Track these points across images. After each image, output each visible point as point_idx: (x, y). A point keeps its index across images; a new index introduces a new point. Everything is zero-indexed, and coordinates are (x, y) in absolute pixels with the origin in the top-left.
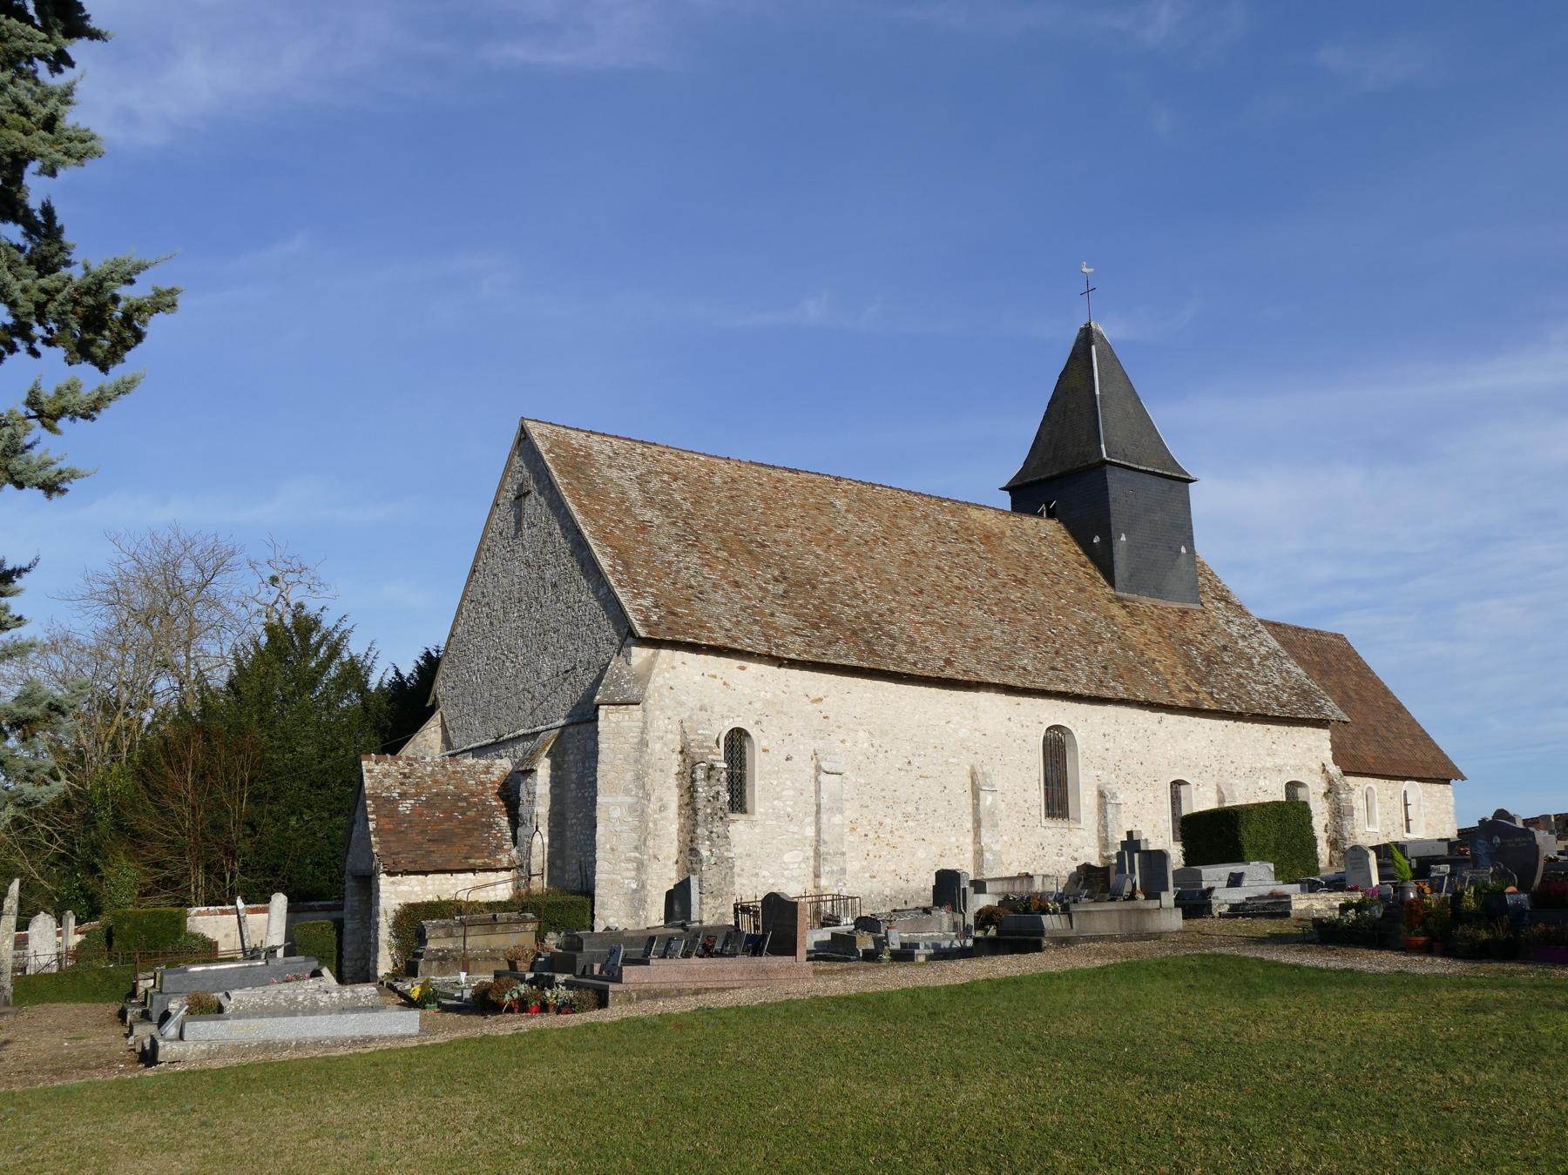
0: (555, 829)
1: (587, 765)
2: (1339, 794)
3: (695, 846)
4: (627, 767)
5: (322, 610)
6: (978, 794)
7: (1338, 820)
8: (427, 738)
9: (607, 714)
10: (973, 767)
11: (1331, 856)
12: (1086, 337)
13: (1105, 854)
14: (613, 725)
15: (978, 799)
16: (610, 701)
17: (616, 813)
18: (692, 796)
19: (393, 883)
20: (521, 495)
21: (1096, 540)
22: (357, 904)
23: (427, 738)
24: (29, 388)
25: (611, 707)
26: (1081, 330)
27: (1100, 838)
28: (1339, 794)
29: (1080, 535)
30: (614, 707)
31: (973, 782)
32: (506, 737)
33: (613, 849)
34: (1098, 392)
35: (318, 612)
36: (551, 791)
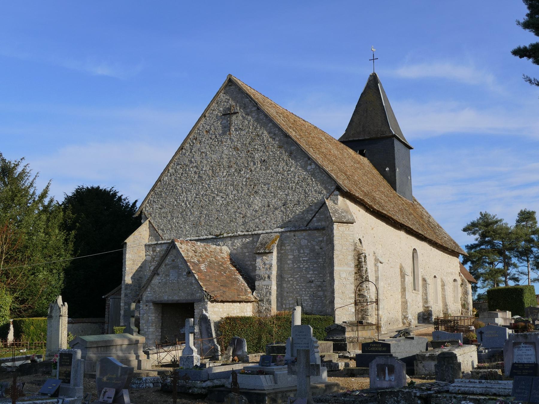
0: (278, 283)
1: (302, 251)
2: (466, 285)
3: (362, 293)
4: (349, 253)
5: (22, 159)
6: (404, 277)
7: (466, 296)
8: (141, 233)
9: (338, 227)
10: (401, 264)
11: (462, 311)
12: (373, 81)
13: (426, 306)
14: (341, 232)
15: (404, 279)
16: (341, 221)
17: (344, 275)
18: (359, 269)
19: (213, 306)
20: (228, 114)
21: (387, 169)
22: (154, 318)
23: (141, 233)
24: (520, 28)
25: (340, 224)
26: (371, 76)
27: (423, 299)
28: (466, 285)
29: (379, 166)
30: (341, 224)
31: (401, 271)
32: (225, 235)
33: (343, 293)
34: (384, 105)
35: (20, 160)
36: (277, 264)
